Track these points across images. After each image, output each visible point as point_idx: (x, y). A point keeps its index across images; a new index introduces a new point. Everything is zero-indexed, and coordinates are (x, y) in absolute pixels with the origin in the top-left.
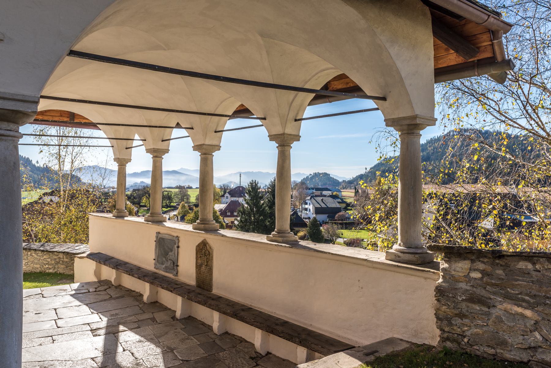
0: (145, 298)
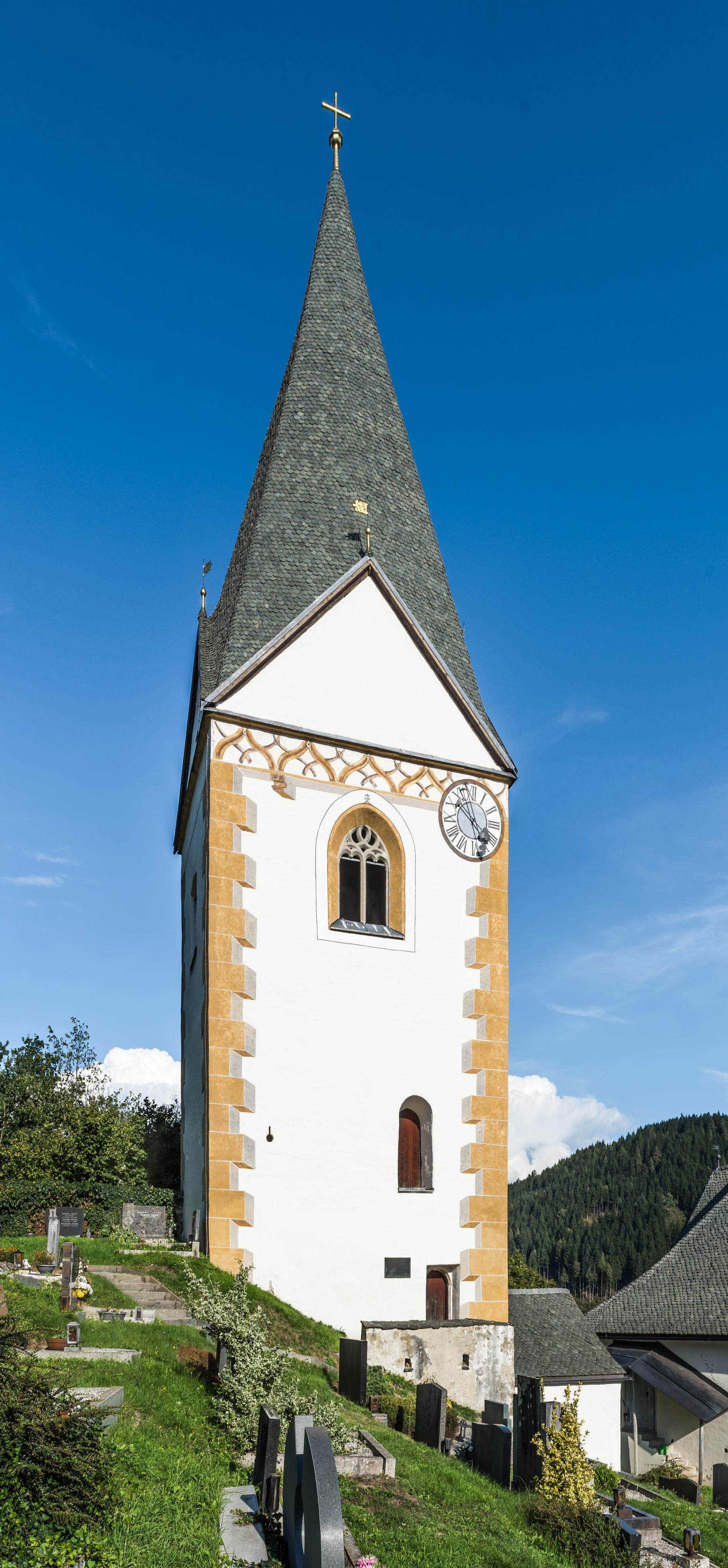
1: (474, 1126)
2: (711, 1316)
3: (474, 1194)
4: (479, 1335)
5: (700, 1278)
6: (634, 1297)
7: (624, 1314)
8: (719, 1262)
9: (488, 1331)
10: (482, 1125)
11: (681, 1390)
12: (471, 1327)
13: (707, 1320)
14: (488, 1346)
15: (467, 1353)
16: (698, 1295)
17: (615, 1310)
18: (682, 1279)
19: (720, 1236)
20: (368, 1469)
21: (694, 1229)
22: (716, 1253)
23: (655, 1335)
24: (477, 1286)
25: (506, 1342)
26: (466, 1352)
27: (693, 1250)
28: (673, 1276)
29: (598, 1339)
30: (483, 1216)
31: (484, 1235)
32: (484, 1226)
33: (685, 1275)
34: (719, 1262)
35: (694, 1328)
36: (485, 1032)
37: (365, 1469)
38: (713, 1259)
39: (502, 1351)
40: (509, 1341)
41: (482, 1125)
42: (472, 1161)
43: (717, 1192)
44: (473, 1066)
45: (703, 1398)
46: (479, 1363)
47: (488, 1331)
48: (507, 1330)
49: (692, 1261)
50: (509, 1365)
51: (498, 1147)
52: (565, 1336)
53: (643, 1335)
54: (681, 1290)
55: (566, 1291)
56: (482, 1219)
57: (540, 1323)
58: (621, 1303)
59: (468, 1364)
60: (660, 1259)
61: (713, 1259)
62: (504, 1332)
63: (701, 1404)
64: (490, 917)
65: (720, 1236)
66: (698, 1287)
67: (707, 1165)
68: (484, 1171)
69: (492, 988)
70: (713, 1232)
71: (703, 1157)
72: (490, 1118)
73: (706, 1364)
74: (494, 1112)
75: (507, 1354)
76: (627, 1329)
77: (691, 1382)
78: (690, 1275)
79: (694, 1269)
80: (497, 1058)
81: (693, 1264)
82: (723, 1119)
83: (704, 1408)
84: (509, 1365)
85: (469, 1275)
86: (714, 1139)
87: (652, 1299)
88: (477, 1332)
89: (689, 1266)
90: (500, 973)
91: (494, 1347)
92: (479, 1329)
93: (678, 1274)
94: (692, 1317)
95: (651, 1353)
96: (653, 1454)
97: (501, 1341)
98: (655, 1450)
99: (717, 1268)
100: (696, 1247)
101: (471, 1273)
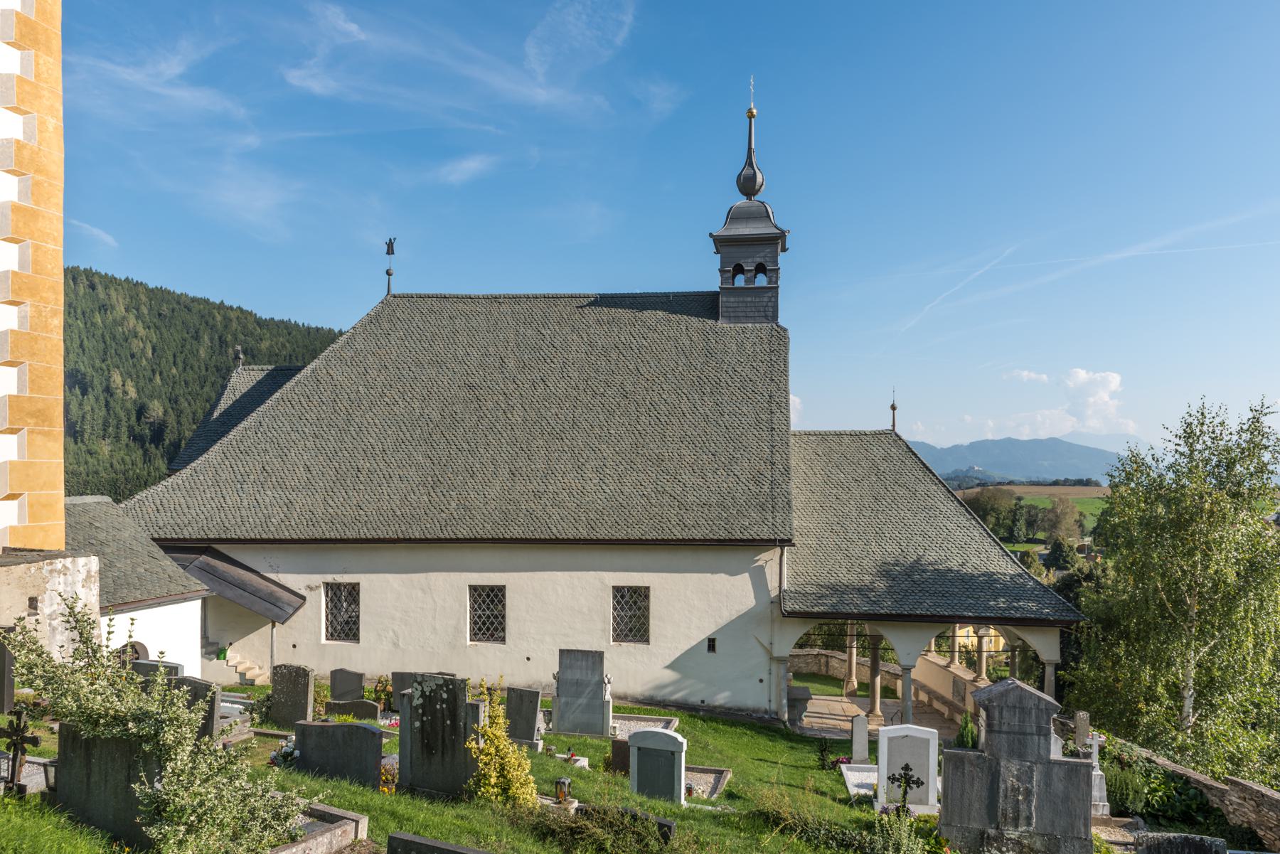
0: (946, 716)
1: (14, 309)
2: (273, 520)
3: (14, 392)
4: (51, 571)
5: (252, 481)
6: (169, 498)
7: (158, 516)
8: (272, 466)
9: (64, 565)
10: (27, 309)
11: (247, 594)
12: (41, 563)
13: (270, 524)
14: (65, 583)
15: (35, 595)
16: (253, 498)
17: (145, 512)
18: (230, 481)
19: (269, 440)
20: (341, 840)
21: (235, 431)
22: (268, 457)
23: (209, 539)
24: (21, 507)
25: (89, 576)
26: (33, 593)
27: (237, 451)
28: (218, 478)
29: (162, 553)
30: (29, 421)
31: (30, 444)
32: (31, 432)
33: (233, 477)
34: (272, 466)
35: (257, 532)
36: (30, 195)
37: (337, 842)
38: (265, 463)
39: (83, 586)
40: (93, 574)
41: (27, 309)
42: (12, 352)
43: (243, 391)
44: (12, 234)
45: (272, 600)
46: (52, 605)
47: (64, 565)
48: (90, 562)
49: (239, 463)
50: (93, 601)
51: (50, 338)
52: (122, 553)
53: (191, 540)
54: (231, 492)
55: (107, 499)
56: (28, 424)
57: (85, 539)
58: (152, 504)
59: (36, 608)
60: (196, 458)
61: (265, 463)
62: (86, 564)
63: (272, 607)
64: (37, 56)
65: (269, 440)
66: (251, 490)
67: (77, 319)
68: (30, 365)
69: (40, 144)
70: (259, 435)
71: (72, 311)
72: (39, 302)
73: (270, 566)
74: (44, 295)
75: (91, 590)
76: (168, 533)
77: (255, 585)
78: (239, 477)
79: (242, 471)
80: (48, 231)
81: (240, 466)
82: (96, 276)
83: (276, 610)
84: (93, 601)
85: (9, 492)
86: (85, 294)
87: (195, 501)
88: (49, 568)
89: (235, 468)
90: (51, 129)
91: (74, 583)
92: (51, 564)
93: (223, 475)
94: (251, 520)
95: (203, 558)
96: (211, 660)
97: (83, 575)
98: (213, 656)
99: (271, 471)
100: (242, 449)
101: (11, 490)
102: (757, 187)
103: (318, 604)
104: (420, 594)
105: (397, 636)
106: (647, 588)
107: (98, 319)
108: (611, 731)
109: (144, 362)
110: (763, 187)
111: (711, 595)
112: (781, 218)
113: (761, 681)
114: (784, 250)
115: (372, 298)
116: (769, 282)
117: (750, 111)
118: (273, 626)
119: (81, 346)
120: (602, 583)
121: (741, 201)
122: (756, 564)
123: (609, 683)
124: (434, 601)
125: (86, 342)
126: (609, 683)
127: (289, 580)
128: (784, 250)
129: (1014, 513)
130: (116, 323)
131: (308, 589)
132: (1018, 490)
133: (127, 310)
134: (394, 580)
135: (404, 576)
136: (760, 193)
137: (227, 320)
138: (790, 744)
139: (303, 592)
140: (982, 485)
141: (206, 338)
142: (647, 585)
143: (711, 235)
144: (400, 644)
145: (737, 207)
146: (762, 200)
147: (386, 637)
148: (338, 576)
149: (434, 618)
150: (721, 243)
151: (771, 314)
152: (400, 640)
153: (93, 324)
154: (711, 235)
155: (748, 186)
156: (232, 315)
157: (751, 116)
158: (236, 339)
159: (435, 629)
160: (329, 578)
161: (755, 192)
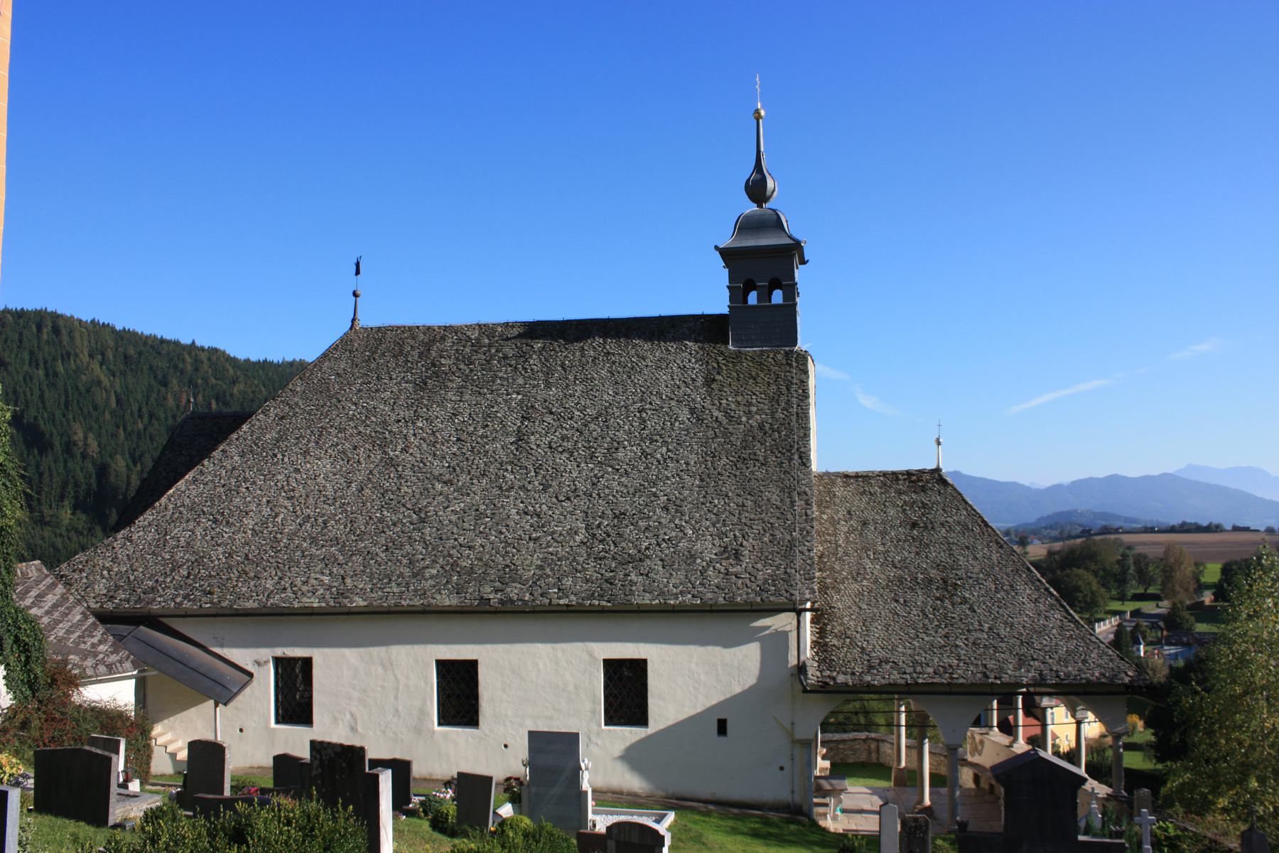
73: (214, 638)
102: (768, 193)
103: (267, 680)
104: (380, 670)
105: (355, 720)
106: (645, 661)
107: (60, 368)
108: (590, 824)
109: (108, 416)
110: (775, 193)
111: (719, 668)
112: (795, 226)
113: (782, 768)
114: (803, 262)
115: (335, 330)
116: (785, 299)
117: (757, 111)
118: (216, 706)
119: (42, 397)
120: (591, 656)
121: (751, 208)
122: (767, 632)
123: (587, 769)
124: (396, 678)
125: (47, 394)
126: (587, 769)
127: (235, 655)
128: (803, 262)
129: (1122, 563)
130: (78, 371)
131: (256, 666)
132: (1126, 538)
133: (91, 356)
134: (351, 655)
135: (362, 650)
136: (772, 200)
137: (197, 364)
138: (730, 823)
139: (250, 668)
140: (1086, 533)
141: (175, 381)
142: (644, 657)
143: (716, 248)
144: (359, 729)
145: (746, 217)
146: (774, 208)
147: (342, 720)
148: (289, 649)
149: (396, 698)
150: (727, 254)
151: (790, 335)
152: (359, 724)
153: (56, 374)
154: (716, 248)
155: (757, 190)
156: (204, 356)
157: (758, 117)
158: (208, 384)
159: (397, 711)
160: (280, 652)
161: (767, 199)
